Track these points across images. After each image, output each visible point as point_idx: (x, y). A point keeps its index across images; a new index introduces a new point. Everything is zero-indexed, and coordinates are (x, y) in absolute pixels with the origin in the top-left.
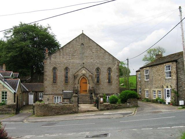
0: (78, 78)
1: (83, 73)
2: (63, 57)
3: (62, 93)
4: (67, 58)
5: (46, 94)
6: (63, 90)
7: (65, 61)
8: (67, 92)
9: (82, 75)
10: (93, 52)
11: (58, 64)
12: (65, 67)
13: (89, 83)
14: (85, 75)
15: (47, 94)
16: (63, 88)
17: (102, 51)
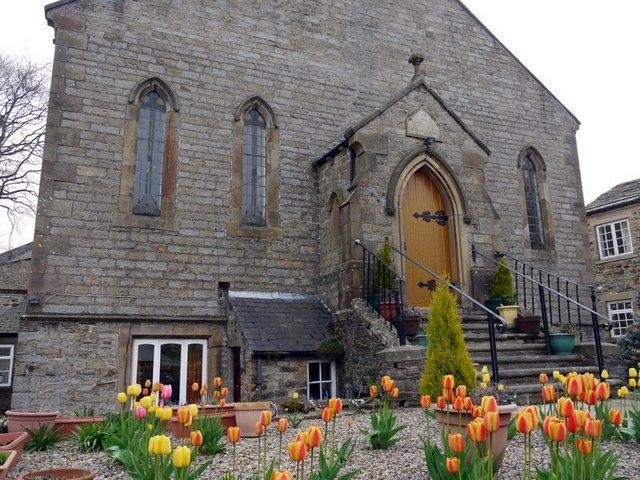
0: (386, 169)
1: (424, 132)
2: (229, 23)
3: (212, 308)
4: (255, 28)
5: (54, 321)
6: (224, 286)
7: (243, 54)
8: (259, 301)
9: (411, 144)
10: (429, 35)
11: (180, 64)
12: (241, 97)
13: (467, 221)
14: (440, 148)
15: (70, 320)
16: (227, 268)
17: (480, 39)
